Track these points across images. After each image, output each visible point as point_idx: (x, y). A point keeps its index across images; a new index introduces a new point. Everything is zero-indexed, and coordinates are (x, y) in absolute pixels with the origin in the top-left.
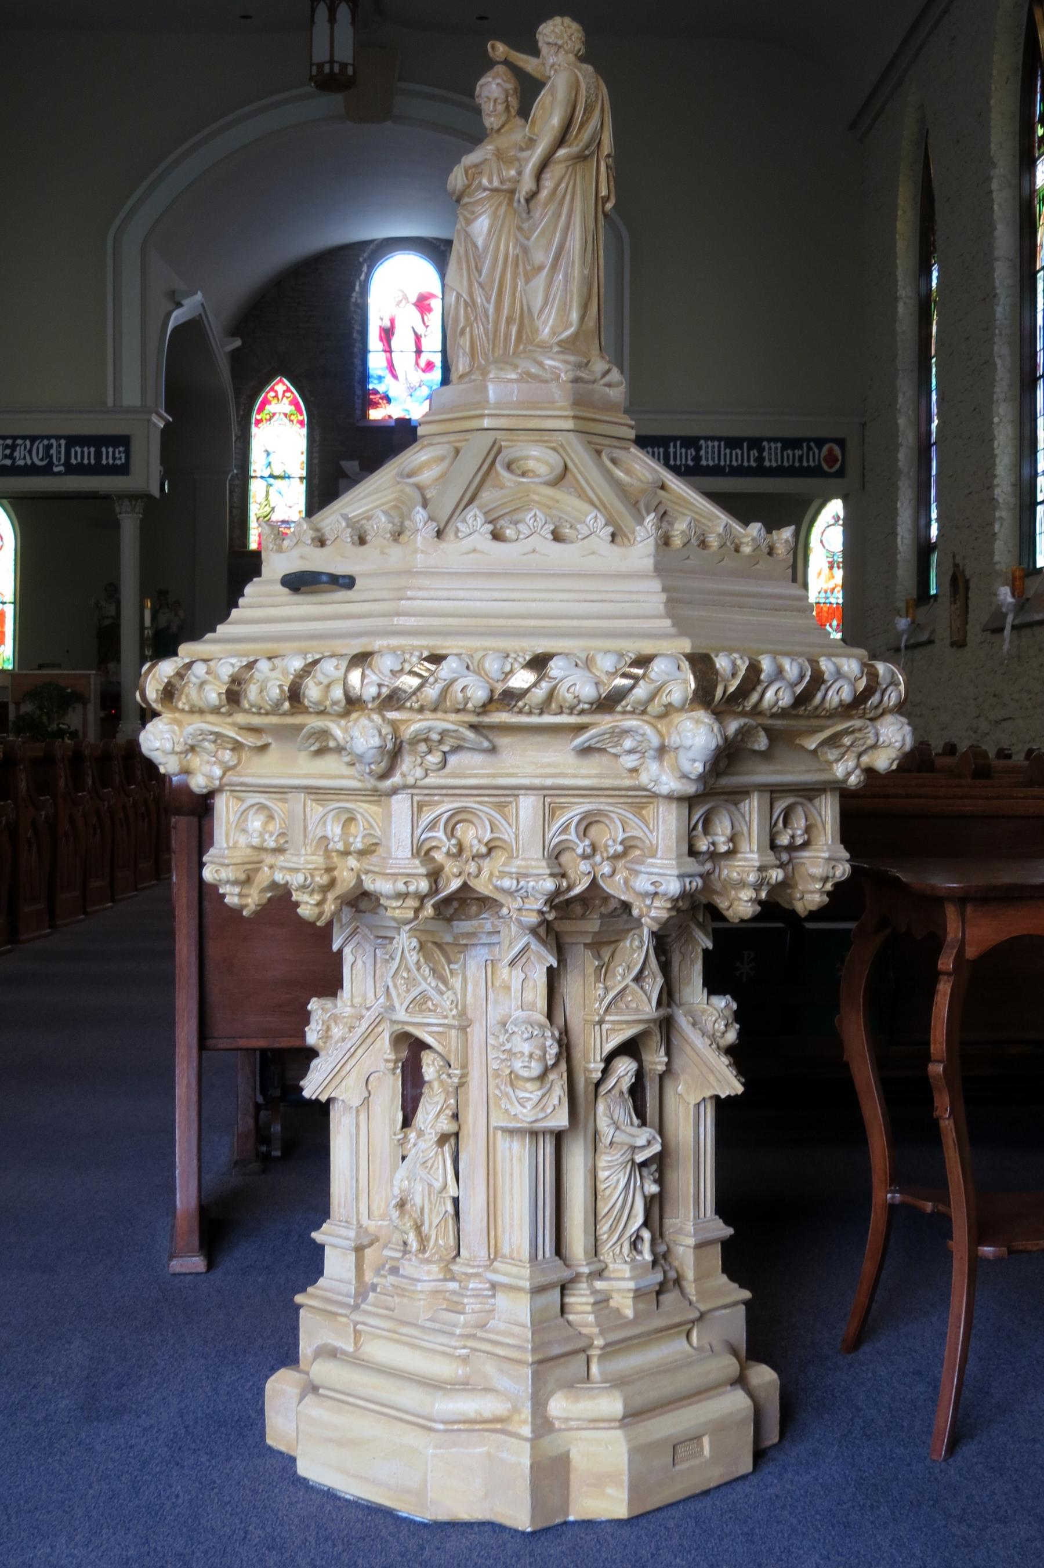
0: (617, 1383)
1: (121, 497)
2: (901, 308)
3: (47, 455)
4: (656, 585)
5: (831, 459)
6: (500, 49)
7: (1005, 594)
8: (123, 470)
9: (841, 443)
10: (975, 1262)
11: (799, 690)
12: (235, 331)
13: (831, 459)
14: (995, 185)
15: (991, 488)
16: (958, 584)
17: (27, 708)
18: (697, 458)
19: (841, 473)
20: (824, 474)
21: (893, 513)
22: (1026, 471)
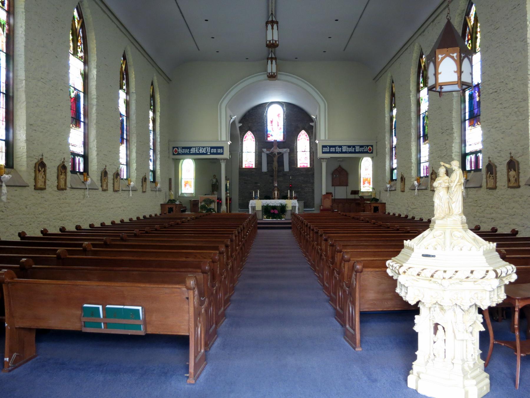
0: (474, 378)
1: (221, 159)
2: (386, 119)
3: (206, 150)
4: (484, 257)
5: (370, 150)
6: (442, 163)
7: (416, 183)
8: (222, 154)
9: (372, 146)
10: (521, 357)
11: (6, 7)
12: (240, 122)
13: (370, 150)
14: (411, 96)
15: (411, 159)
16: (403, 179)
17: (203, 204)
18: (342, 150)
19: (372, 153)
20: (369, 153)
21: (385, 162)
22: (419, 156)
